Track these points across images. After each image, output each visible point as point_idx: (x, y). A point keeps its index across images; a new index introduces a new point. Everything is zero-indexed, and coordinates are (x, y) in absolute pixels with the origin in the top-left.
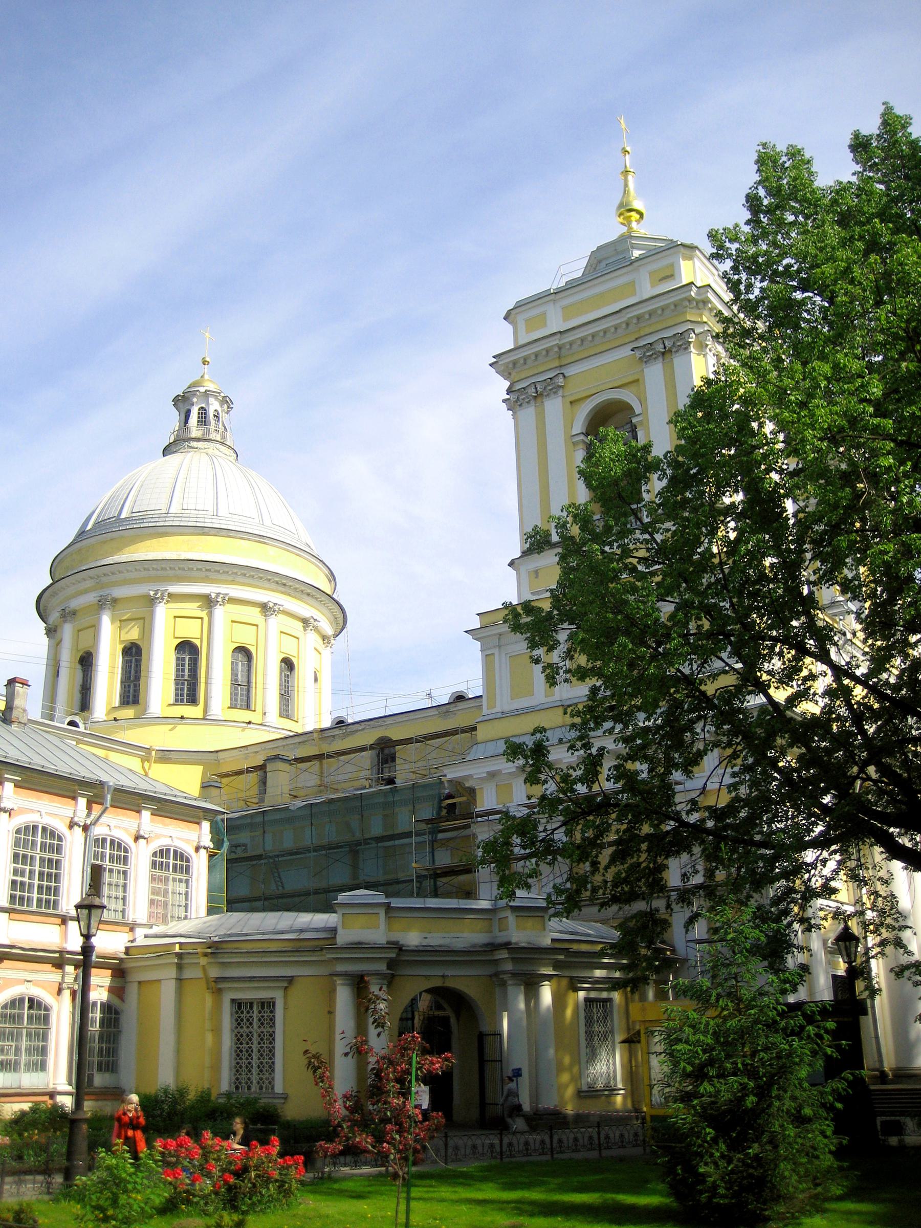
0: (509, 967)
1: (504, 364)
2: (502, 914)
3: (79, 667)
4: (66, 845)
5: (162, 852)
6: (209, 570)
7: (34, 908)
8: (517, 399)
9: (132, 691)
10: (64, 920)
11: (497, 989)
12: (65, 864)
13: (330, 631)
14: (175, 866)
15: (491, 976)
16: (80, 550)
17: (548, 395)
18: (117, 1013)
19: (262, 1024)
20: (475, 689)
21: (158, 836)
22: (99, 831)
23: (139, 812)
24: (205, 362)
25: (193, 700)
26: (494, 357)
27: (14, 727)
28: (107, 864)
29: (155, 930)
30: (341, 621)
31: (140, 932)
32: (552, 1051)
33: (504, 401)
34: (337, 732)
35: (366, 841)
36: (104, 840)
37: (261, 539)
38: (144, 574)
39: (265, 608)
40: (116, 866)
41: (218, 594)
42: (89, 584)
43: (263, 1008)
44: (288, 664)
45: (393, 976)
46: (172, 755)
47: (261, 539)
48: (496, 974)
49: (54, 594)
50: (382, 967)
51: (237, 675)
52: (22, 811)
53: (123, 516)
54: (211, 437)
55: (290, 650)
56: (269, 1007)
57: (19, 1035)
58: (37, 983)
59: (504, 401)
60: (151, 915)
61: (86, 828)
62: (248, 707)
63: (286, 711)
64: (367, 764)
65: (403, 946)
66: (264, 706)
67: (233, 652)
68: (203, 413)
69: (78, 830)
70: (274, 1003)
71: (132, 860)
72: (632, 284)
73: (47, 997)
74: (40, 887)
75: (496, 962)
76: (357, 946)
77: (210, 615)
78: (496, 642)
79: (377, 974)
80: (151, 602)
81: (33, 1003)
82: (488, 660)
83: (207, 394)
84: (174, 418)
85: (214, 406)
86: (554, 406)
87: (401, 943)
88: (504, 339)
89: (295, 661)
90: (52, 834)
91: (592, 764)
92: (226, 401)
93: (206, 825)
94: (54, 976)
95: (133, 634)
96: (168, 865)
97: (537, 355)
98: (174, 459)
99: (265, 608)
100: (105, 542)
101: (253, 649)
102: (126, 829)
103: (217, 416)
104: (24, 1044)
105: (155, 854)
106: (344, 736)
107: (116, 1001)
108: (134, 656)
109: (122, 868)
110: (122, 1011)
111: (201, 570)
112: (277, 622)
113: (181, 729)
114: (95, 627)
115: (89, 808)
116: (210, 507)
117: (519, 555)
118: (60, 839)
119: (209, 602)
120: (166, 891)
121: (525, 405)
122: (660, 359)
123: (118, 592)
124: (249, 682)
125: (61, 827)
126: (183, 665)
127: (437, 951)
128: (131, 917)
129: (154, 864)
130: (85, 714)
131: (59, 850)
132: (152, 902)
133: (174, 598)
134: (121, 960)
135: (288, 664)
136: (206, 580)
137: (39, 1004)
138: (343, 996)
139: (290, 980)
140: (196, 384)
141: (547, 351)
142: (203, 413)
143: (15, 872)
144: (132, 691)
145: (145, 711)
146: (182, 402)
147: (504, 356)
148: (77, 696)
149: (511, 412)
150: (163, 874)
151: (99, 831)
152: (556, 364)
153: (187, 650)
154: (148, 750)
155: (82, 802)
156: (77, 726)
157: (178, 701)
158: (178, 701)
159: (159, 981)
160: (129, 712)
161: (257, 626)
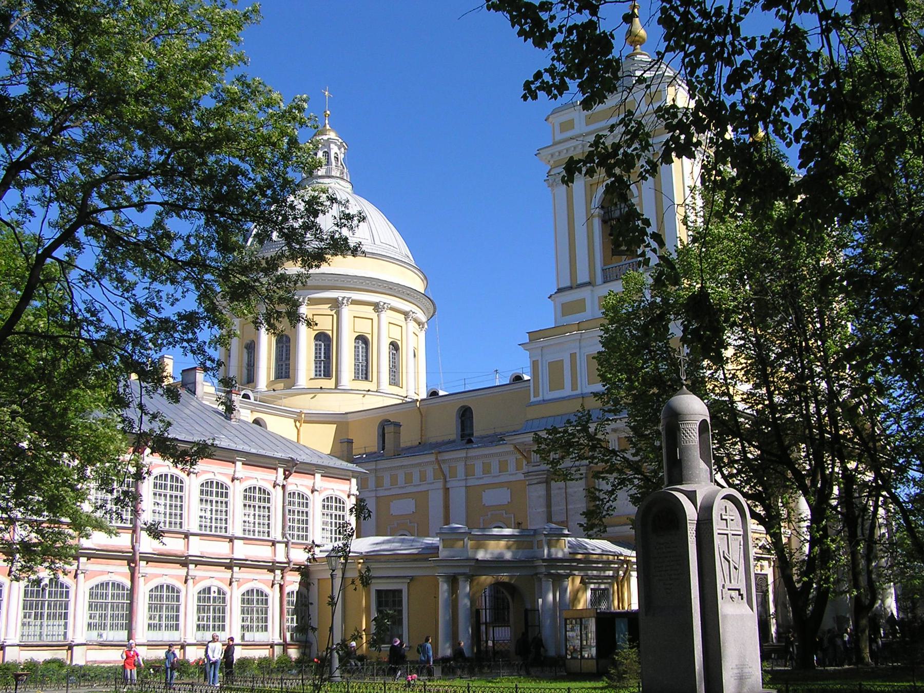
3: (245, 351)
4: (272, 497)
21: (325, 489)
22: (290, 488)
23: (313, 475)
25: (328, 375)
36: (294, 493)
39: (377, 307)
41: (344, 298)
52: (248, 478)
54: (333, 174)
57: (161, 608)
62: (366, 379)
63: (395, 379)
67: (356, 339)
69: (279, 489)
73: (267, 589)
77: (338, 314)
79: (464, 574)
81: (260, 593)
93: (354, 481)
94: (270, 576)
99: (377, 307)
102: (307, 486)
104: (164, 613)
105: (324, 500)
107: (305, 591)
124: (367, 361)
125: (269, 487)
126: (320, 349)
135: (394, 346)
139: (412, 578)
157: (318, 375)
158: (318, 375)
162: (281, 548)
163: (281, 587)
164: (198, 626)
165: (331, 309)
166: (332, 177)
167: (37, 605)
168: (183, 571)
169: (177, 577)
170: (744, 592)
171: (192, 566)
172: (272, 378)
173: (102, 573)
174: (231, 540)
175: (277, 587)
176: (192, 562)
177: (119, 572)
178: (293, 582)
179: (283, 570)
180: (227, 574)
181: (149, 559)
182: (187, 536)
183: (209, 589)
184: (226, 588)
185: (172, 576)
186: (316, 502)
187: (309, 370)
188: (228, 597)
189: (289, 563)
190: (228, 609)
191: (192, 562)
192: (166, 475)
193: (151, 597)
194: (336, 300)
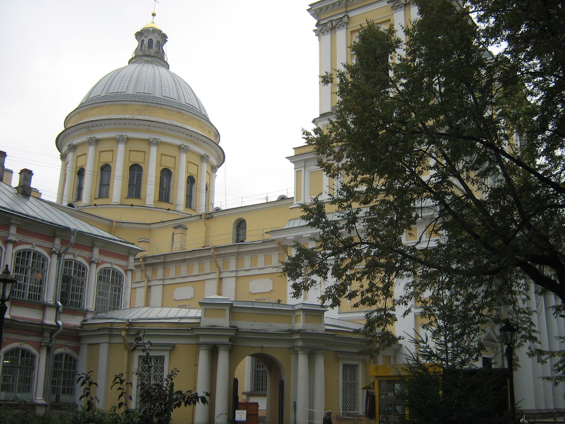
0: (300, 344)
2: (297, 314)
5: (106, 271)
6: (150, 126)
8: (322, 29)
11: (293, 356)
14: (112, 279)
15: (290, 349)
17: (339, 27)
18: (75, 361)
19: (156, 370)
20: (291, 194)
26: (310, 5)
31: (89, 316)
32: (407, 413)
33: (314, 31)
43: (157, 361)
45: (233, 346)
48: (293, 348)
49: (65, 137)
50: (227, 341)
51: (163, 184)
56: (160, 361)
58: (26, 342)
59: (314, 31)
61: (59, 255)
65: (239, 329)
69: (55, 257)
70: (164, 359)
75: (293, 341)
76: (213, 328)
78: (303, 164)
79: (224, 344)
82: (298, 173)
86: (341, 35)
87: (238, 327)
91: (352, 219)
102: (84, 258)
110: (78, 360)
111: (145, 125)
117: (318, 116)
121: (326, 33)
122: (403, 8)
127: (259, 333)
135: (191, 180)
138: (203, 357)
147: (315, 5)
148: (76, 192)
149: (317, 37)
152: (344, 10)
156: (74, 207)
157: (130, 196)
158: (130, 196)
159: (99, 344)
161: (175, 157)
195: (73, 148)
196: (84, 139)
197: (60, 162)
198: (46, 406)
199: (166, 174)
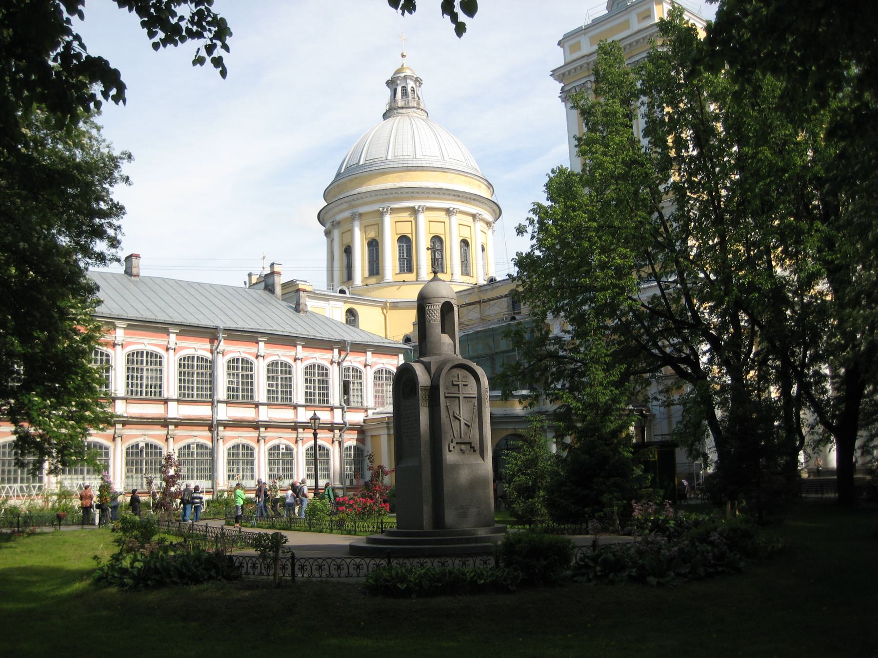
1: (558, 74)
3: (344, 255)
4: (330, 373)
7: (317, 404)
9: (375, 267)
10: (332, 409)
12: (330, 382)
13: (490, 218)
16: (338, 185)
18: (362, 451)
21: (376, 364)
22: (345, 364)
24: (403, 56)
25: (410, 270)
27: (301, 314)
28: (351, 380)
29: (378, 410)
30: (498, 211)
31: (370, 412)
34: (488, 287)
35: (497, 353)
36: (349, 368)
37: (443, 170)
38: (375, 198)
39: (448, 211)
40: (356, 381)
41: (419, 206)
42: (345, 206)
44: (465, 243)
46: (399, 304)
47: (443, 170)
49: (326, 213)
53: (361, 163)
55: (466, 234)
60: (375, 403)
61: (339, 364)
64: (505, 305)
66: (451, 270)
68: (404, 89)
69: (335, 365)
71: (364, 377)
72: (627, 21)
74: (319, 394)
77: (416, 219)
80: (381, 214)
83: (405, 78)
84: (388, 92)
85: (411, 84)
88: (558, 58)
89: (469, 240)
90: (323, 368)
92: (418, 81)
94: (330, 435)
95: (372, 235)
96: (382, 378)
97: (575, 69)
98: (390, 121)
100: (351, 180)
101: (443, 237)
102: (360, 362)
103: (413, 91)
106: (493, 288)
107: (361, 445)
108: (374, 246)
109: (359, 381)
112: (456, 219)
113: (404, 288)
114: (351, 231)
115: (340, 353)
116: (411, 153)
118: (327, 370)
119: (414, 211)
120: (383, 391)
123: (362, 210)
125: (327, 364)
128: (365, 404)
129: (375, 378)
130: (350, 282)
131: (327, 375)
132: (375, 396)
133: (394, 211)
134: (361, 426)
135: (465, 243)
136: (412, 198)
137: (324, 448)
140: (398, 71)
141: (581, 66)
142: (404, 89)
143: (307, 388)
144: (375, 267)
145: (383, 279)
146: (391, 84)
148: (345, 272)
150: (381, 382)
151: (345, 364)
153: (404, 241)
154: (385, 303)
155: (336, 351)
157: (402, 271)
158: (402, 271)
160: (373, 280)
162: (338, 412)
163: (340, 443)
164: (229, 476)
165: (410, 215)
166: (409, 107)
167: (137, 462)
168: (255, 434)
169: (251, 438)
170: (477, 447)
171: (300, 430)
172: (367, 274)
173: (136, 436)
174: (295, 407)
175: (336, 443)
176: (263, 426)
177: (202, 436)
178: (351, 440)
179: (340, 429)
180: (293, 435)
181: (226, 425)
182: (257, 405)
183: (278, 446)
184: (292, 445)
185: (246, 438)
186: (368, 376)
187: (394, 266)
188: (294, 452)
189: (345, 424)
190: (295, 461)
191: (263, 426)
192: (238, 359)
193: (229, 454)
194: (413, 208)
195: (336, 224)
196: (347, 214)
197: (324, 239)
198: (343, 489)
199: (437, 242)
